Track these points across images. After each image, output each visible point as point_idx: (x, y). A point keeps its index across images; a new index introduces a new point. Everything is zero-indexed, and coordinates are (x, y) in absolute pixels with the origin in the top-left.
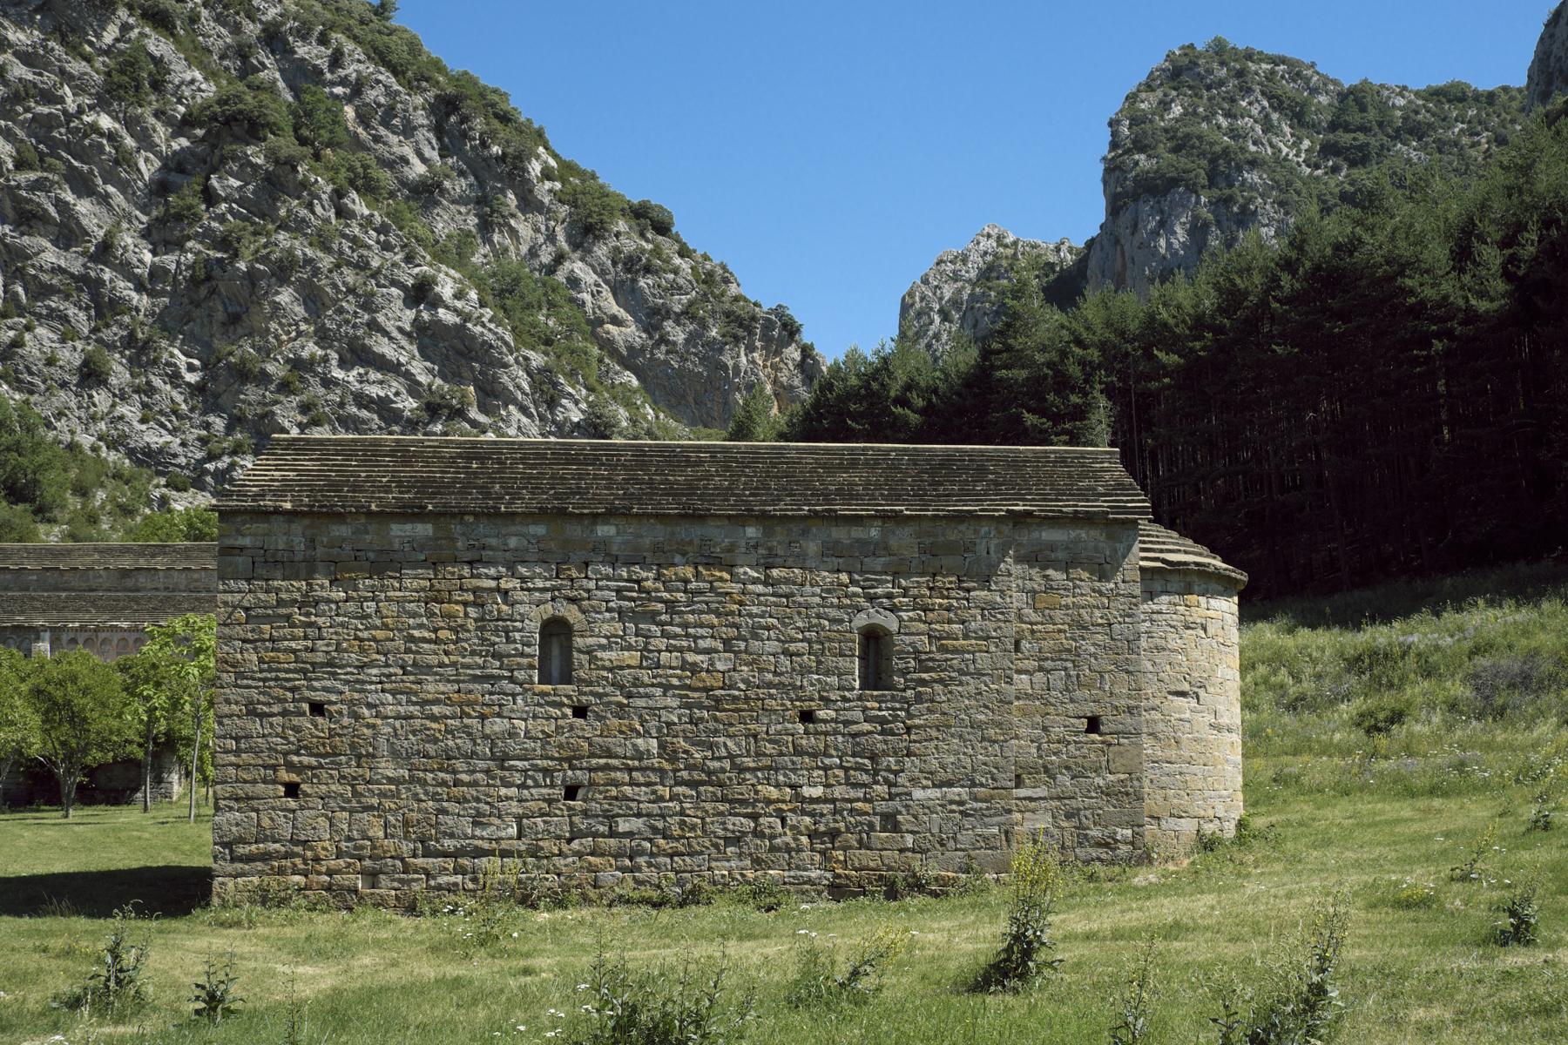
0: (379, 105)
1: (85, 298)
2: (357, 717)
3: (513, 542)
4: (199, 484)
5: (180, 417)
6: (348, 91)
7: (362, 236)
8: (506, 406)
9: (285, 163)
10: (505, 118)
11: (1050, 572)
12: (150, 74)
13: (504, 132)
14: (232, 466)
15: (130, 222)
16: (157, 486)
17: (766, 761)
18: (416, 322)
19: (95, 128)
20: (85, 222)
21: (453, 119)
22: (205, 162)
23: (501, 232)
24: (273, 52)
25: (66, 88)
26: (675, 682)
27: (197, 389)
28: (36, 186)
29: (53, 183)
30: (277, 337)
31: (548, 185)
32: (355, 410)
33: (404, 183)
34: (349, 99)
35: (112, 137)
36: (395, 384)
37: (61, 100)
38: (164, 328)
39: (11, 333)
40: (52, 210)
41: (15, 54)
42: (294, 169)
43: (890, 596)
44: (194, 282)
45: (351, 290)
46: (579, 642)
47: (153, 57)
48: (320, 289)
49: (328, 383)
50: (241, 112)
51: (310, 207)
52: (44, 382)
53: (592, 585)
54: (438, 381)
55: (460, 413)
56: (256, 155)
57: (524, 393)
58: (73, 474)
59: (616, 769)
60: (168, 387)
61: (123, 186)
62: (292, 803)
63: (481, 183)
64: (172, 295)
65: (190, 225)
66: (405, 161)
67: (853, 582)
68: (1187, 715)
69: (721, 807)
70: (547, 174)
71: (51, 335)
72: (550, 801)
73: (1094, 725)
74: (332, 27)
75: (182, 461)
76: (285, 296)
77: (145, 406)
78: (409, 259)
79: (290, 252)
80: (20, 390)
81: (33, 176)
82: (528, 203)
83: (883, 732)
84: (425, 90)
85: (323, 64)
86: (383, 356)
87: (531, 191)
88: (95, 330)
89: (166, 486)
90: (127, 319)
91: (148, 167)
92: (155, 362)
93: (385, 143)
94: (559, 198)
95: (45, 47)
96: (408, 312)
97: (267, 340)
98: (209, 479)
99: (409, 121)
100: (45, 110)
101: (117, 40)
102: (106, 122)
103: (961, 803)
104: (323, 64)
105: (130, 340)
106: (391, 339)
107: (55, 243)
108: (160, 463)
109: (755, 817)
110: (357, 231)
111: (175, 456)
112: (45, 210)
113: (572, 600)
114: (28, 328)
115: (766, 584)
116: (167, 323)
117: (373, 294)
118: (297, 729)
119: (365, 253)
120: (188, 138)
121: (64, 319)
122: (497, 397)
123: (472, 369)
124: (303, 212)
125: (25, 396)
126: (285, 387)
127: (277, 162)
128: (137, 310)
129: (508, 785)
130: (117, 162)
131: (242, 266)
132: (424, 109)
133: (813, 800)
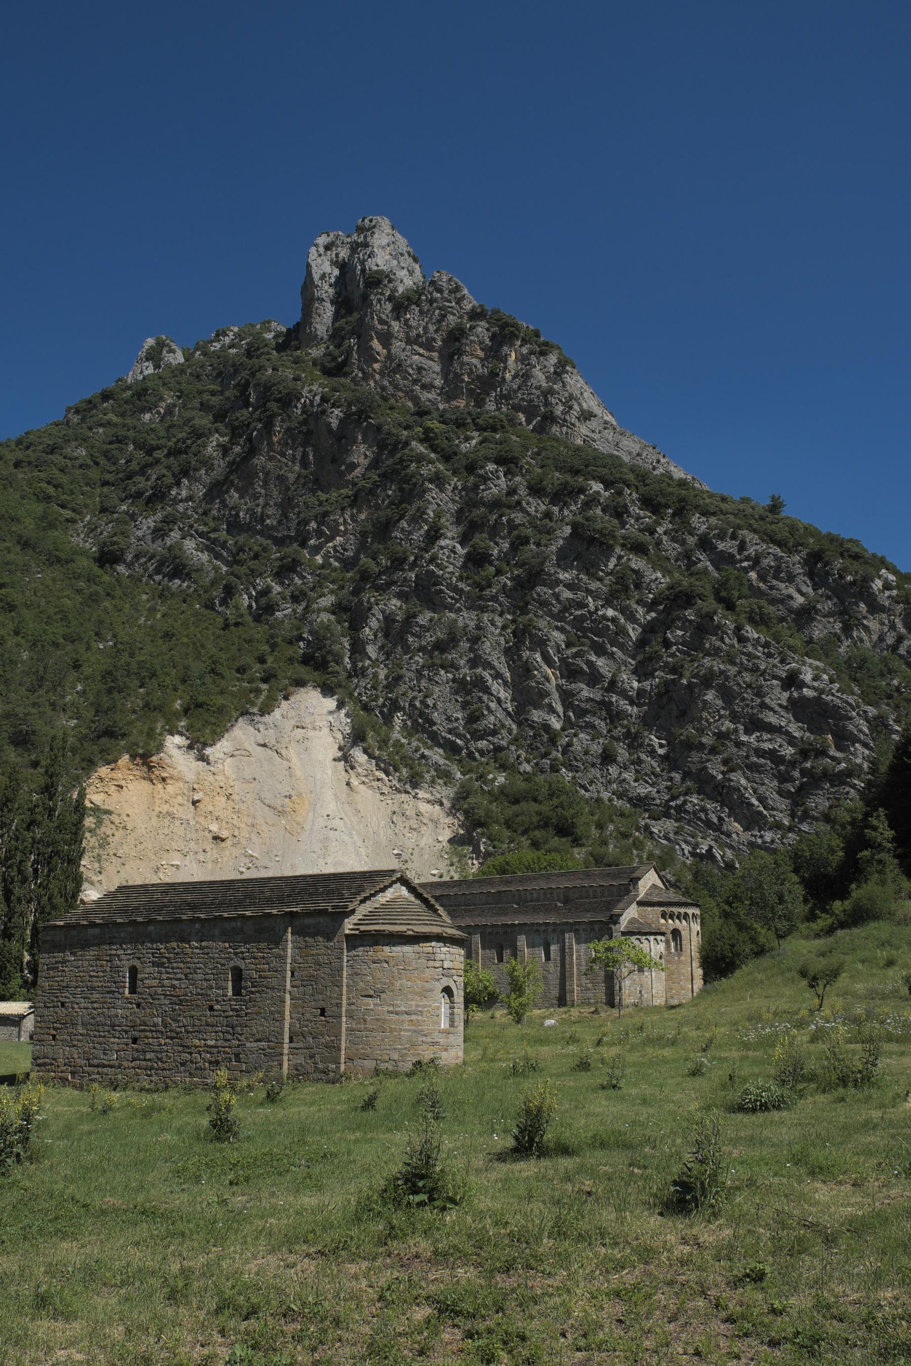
0: (771, 567)
1: (604, 713)
2: (73, 1008)
3: (122, 935)
4: (667, 815)
5: (656, 776)
6: (751, 563)
7: (754, 651)
8: (853, 745)
9: (706, 616)
10: (856, 557)
11: (307, 939)
12: (633, 580)
13: (856, 565)
14: (685, 802)
15: (626, 666)
16: (644, 819)
17: (196, 1028)
18: (790, 699)
19: (604, 617)
20: (601, 671)
21: (819, 565)
22: (664, 624)
23: (858, 629)
24: (705, 551)
25: (590, 598)
26: (168, 993)
27: (665, 758)
28: (576, 655)
29: (585, 652)
30: (707, 721)
31: (887, 593)
32: (755, 759)
33: (791, 611)
34: (752, 568)
35: (614, 620)
36: (779, 740)
37: (587, 606)
38: (645, 725)
39: (567, 739)
40: (585, 667)
41: (565, 586)
42: (712, 619)
43: (242, 953)
44: (659, 695)
45: (749, 686)
46: (139, 976)
47: (633, 570)
48: (730, 688)
49: (739, 744)
50: (680, 592)
51: (722, 640)
52: (583, 764)
53: (145, 952)
54: (808, 734)
55: (823, 753)
56: (690, 615)
57: (865, 734)
58: (596, 818)
59: (147, 1031)
60: (649, 759)
61: (621, 647)
62: (53, 1043)
63: (842, 602)
64: (649, 704)
65: (657, 662)
66: (790, 597)
67: (230, 947)
68: (372, 1007)
69: (180, 1049)
70: (887, 586)
71: (587, 737)
72: (126, 1045)
73: (323, 1012)
74: (739, 527)
75: (658, 802)
76: (710, 696)
77: (637, 771)
78: (783, 661)
79: (710, 668)
80: (571, 771)
81: (574, 650)
82: (875, 608)
83: (237, 1016)
84: (801, 551)
85: (734, 551)
86: (771, 723)
87: (875, 600)
88: (609, 731)
89: (648, 818)
90: (625, 722)
91: (634, 633)
92: (641, 745)
93: (777, 589)
94: (895, 600)
95: (578, 579)
96: (784, 694)
97: (702, 724)
98: (672, 811)
99: (790, 573)
100: (579, 613)
101: (616, 565)
102: (610, 613)
103: (264, 1050)
104: (734, 551)
105: (628, 734)
106: (775, 712)
107: (588, 685)
108: (646, 805)
109: (191, 1053)
110: (750, 649)
111: (654, 799)
112: (581, 668)
113: (139, 958)
114: (576, 735)
115: (200, 949)
116: (647, 722)
117: (761, 686)
118: (56, 1013)
119: (756, 661)
120: (655, 612)
121: (593, 727)
122: (847, 740)
123: (829, 723)
124: (718, 643)
125: (573, 774)
126: (713, 751)
127: (701, 617)
128: (631, 716)
129: (114, 1037)
130: (617, 634)
131: (684, 681)
132: (800, 563)
133: (212, 1047)
